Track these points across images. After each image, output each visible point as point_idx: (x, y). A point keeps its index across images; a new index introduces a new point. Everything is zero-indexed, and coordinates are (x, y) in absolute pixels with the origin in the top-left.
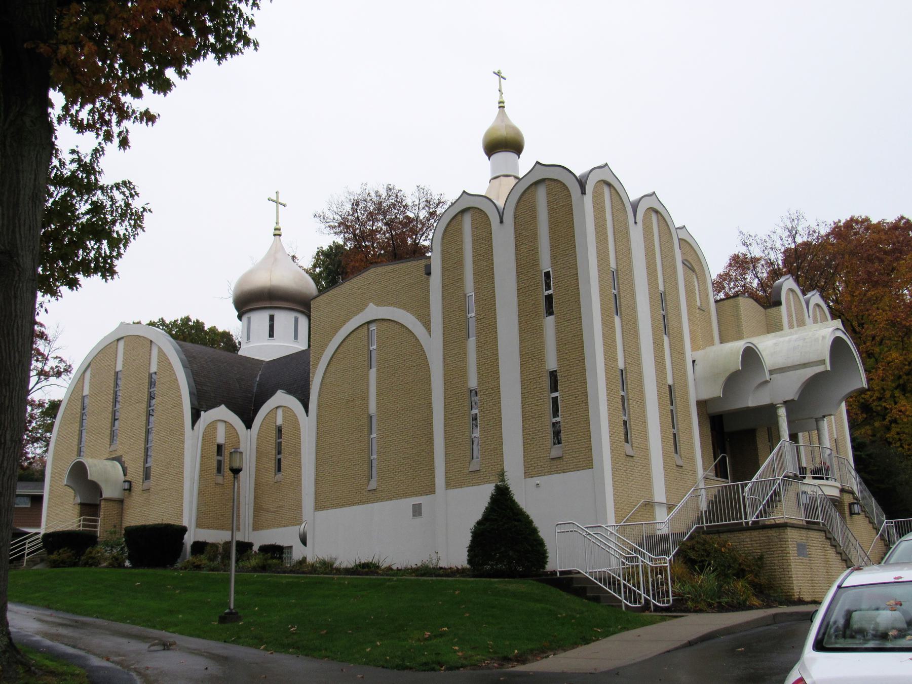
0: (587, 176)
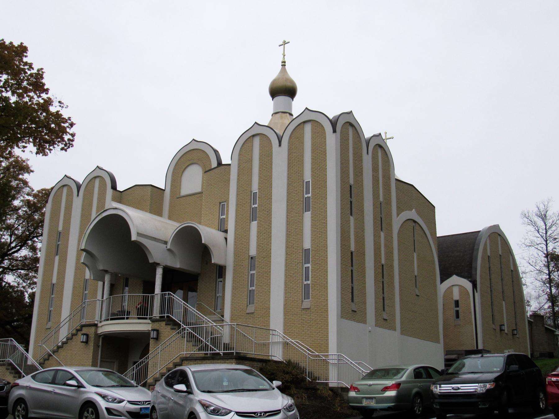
0: (337, 118)
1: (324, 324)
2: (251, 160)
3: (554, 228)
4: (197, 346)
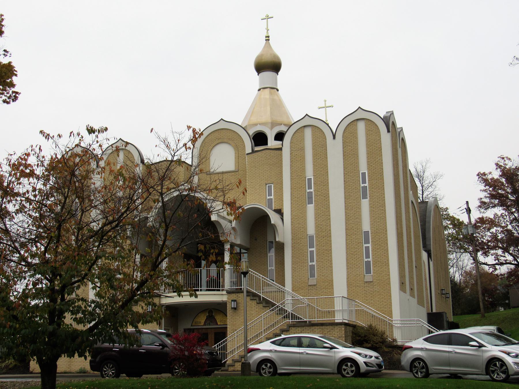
1: (387, 295)
2: (303, 149)
3: (430, 189)
4: (282, 314)
